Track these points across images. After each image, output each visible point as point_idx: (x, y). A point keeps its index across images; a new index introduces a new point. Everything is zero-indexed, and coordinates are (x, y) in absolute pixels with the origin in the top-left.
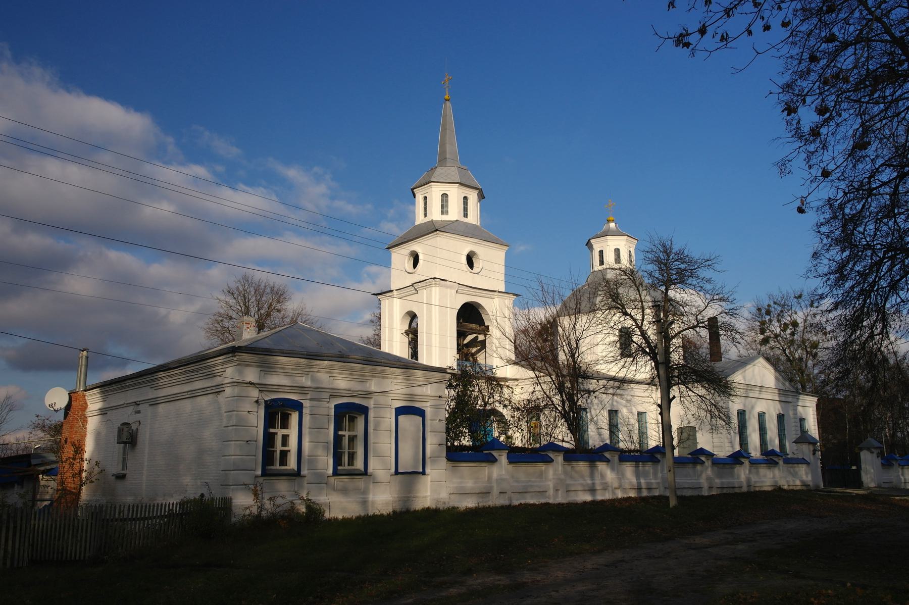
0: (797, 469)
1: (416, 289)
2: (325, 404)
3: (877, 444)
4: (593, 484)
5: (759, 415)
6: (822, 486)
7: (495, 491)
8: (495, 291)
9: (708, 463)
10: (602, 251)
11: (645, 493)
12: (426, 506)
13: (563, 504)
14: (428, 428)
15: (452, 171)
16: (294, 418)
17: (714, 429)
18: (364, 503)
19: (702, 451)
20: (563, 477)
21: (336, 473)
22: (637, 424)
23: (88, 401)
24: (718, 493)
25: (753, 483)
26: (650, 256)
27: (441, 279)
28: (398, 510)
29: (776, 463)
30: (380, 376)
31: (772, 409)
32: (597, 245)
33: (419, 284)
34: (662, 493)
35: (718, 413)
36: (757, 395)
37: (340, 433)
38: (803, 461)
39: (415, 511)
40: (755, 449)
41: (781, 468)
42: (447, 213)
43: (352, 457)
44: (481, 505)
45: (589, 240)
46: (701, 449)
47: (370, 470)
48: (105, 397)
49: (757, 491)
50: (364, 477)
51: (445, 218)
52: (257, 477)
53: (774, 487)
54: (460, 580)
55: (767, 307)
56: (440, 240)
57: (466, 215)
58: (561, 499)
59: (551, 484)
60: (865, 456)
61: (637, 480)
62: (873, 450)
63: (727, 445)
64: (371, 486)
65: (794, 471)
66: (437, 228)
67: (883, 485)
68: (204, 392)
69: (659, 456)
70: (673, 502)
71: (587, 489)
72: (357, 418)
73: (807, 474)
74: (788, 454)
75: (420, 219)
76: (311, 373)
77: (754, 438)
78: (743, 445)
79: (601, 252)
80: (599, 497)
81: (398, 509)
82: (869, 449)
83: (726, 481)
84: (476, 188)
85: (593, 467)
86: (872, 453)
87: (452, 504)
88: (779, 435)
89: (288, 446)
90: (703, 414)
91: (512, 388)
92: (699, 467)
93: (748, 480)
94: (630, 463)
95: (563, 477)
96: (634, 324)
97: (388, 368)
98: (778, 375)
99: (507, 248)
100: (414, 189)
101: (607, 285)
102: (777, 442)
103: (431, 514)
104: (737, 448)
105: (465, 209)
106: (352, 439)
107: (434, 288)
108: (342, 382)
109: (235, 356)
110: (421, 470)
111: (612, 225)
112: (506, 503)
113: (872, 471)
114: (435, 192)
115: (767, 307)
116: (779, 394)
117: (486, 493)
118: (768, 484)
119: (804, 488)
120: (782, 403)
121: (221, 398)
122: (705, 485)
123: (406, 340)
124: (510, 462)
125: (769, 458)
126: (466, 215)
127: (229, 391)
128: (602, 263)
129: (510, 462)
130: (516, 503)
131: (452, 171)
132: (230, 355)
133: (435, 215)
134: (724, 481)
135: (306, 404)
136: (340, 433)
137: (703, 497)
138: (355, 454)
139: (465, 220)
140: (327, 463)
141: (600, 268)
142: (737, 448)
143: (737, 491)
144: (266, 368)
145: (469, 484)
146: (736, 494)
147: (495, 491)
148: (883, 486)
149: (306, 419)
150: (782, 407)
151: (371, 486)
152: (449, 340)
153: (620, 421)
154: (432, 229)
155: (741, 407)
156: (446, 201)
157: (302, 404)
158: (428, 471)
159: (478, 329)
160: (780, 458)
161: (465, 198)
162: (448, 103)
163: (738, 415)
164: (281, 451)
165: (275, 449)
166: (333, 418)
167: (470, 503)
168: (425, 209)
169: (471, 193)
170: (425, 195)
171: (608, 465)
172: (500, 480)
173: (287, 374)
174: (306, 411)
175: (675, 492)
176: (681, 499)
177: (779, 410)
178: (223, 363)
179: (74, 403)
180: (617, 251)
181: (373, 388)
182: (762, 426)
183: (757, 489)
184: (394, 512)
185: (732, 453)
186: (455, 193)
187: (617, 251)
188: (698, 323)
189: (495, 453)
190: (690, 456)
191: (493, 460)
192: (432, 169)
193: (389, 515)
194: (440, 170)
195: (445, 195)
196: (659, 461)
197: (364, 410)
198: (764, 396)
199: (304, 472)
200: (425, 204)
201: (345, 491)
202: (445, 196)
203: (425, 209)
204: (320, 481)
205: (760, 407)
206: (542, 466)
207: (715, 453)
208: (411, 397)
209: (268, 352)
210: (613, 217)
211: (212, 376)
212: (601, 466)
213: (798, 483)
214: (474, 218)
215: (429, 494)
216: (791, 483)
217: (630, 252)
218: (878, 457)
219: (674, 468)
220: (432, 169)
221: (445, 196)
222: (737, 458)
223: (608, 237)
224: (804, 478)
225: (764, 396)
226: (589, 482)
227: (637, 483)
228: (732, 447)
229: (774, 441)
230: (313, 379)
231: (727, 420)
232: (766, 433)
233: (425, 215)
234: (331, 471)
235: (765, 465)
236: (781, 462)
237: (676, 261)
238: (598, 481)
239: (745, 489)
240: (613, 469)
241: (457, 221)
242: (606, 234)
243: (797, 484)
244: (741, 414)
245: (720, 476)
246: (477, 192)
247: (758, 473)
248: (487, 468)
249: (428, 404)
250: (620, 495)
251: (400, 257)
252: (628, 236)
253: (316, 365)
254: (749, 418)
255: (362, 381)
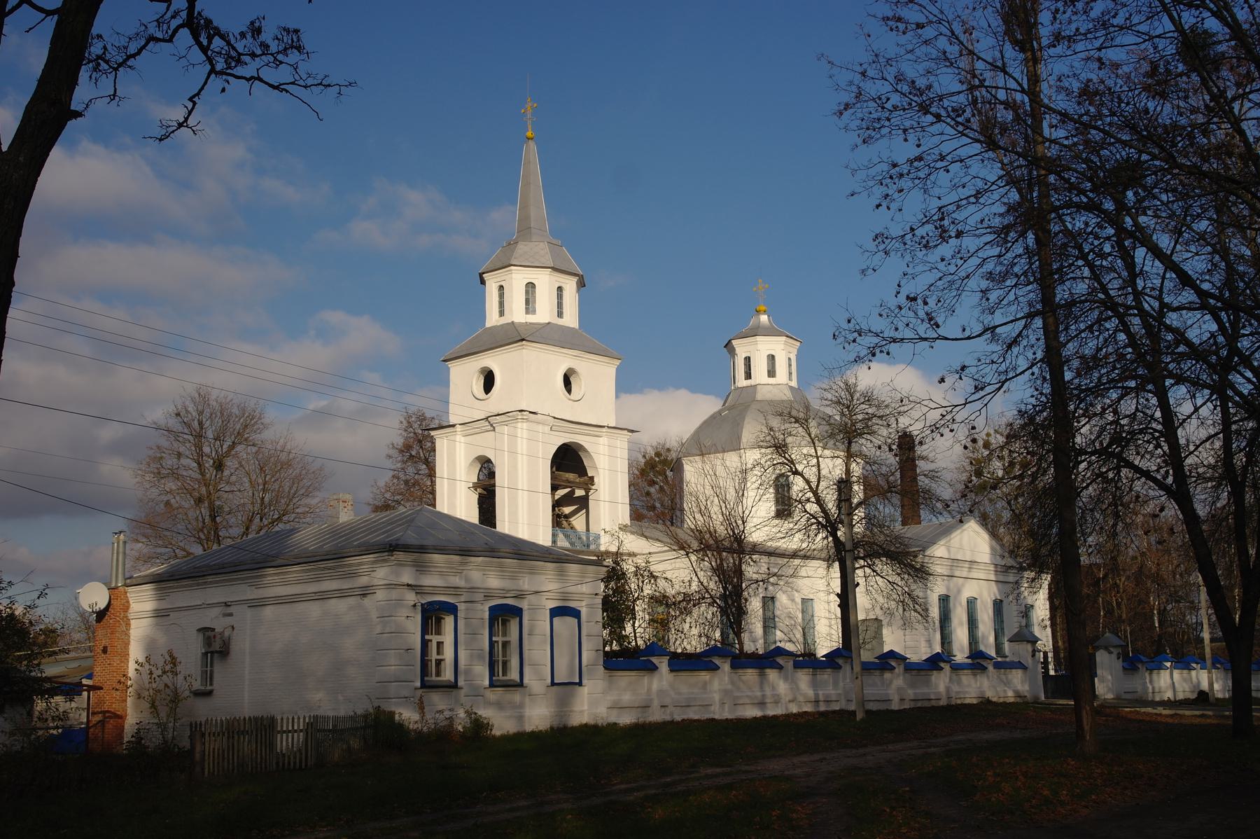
0: (1010, 677)
1: (492, 425)
2: (479, 606)
3: (1116, 641)
4: (764, 696)
5: (968, 602)
6: (1043, 698)
7: (656, 703)
8: (604, 427)
9: (899, 669)
10: (749, 358)
11: (822, 708)
12: (584, 722)
13: (731, 720)
14: (584, 633)
15: (539, 248)
16: (448, 622)
17: (906, 624)
18: (521, 718)
19: (892, 654)
20: (730, 687)
21: (492, 685)
22: (800, 616)
23: (130, 599)
24: (912, 706)
25: (953, 695)
26: (830, 396)
27: (530, 412)
28: (555, 726)
29: (984, 669)
30: (533, 572)
31: (985, 594)
32: (742, 348)
33: (497, 417)
34: (844, 707)
35: (911, 604)
36: (965, 574)
37: (427, 637)
38: (1020, 666)
39: (573, 728)
40: (962, 651)
41: (990, 674)
42: (534, 312)
43: (505, 664)
44: (641, 720)
45: (730, 341)
46: (892, 652)
47: (526, 681)
48: (161, 596)
49: (959, 705)
50: (520, 689)
51: (531, 319)
52: (416, 689)
53: (980, 700)
54: (632, 798)
55: (985, 437)
56: (529, 354)
57: (560, 314)
58: (727, 714)
59: (717, 697)
60: (1101, 657)
61: (814, 690)
62: (1112, 649)
63: (923, 644)
64: (527, 699)
65: (1007, 678)
66: (523, 337)
67: (1124, 696)
68: (342, 594)
69: (840, 661)
70: (860, 716)
71: (756, 702)
72: (509, 621)
73: (1022, 682)
74: (1006, 657)
75: (493, 319)
76: (465, 572)
77: (960, 635)
78: (946, 645)
79: (748, 360)
80: (771, 712)
81: (555, 724)
82: (1106, 648)
83: (922, 691)
84: (575, 275)
85: (762, 675)
86: (1110, 653)
87: (613, 719)
88: (995, 629)
89: (443, 654)
90: (893, 605)
91: (671, 581)
92: (887, 675)
93: (948, 689)
94: (807, 670)
95: (730, 687)
96: (807, 487)
97: (542, 563)
98: (994, 543)
99: (618, 362)
100: (484, 273)
101: (772, 433)
102: (992, 639)
103: (591, 732)
104: (938, 649)
105: (560, 305)
106: (505, 644)
107: (519, 425)
108: (494, 582)
109: (392, 556)
110: (578, 681)
111: (764, 318)
112: (668, 718)
113: (1110, 677)
114: (517, 279)
115: (985, 437)
116: (996, 571)
117: (645, 707)
118: (974, 695)
119: (1018, 700)
120: (1000, 585)
121: (367, 601)
122: (896, 698)
123: (475, 497)
124: (672, 671)
125: (976, 661)
126: (560, 314)
127: (380, 595)
128: (748, 375)
129: (672, 671)
130: (678, 718)
131: (539, 248)
132: (386, 554)
133: (517, 313)
134: (917, 691)
135: (461, 607)
136: (427, 637)
137: (892, 711)
138: (508, 663)
139: (560, 322)
140: (482, 673)
141: (748, 382)
142: (938, 649)
143: (934, 703)
144: (421, 568)
145: (627, 698)
146: (933, 707)
147: (656, 703)
148: (1123, 697)
149: (461, 623)
150: (999, 590)
151: (527, 699)
152: (445, 464)
153: (777, 613)
154: (514, 336)
155: (943, 591)
156: (532, 294)
157: (457, 606)
158: (584, 682)
159: (578, 480)
160: (989, 661)
161: (560, 289)
162: (531, 143)
163: (939, 602)
164: (436, 660)
165: (429, 658)
166: (487, 621)
167: (626, 719)
168: (501, 304)
169: (567, 281)
170: (502, 283)
171: (780, 672)
172: (661, 692)
173: (441, 574)
174: (461, 614)
175: (863, 705)
176: (868, 712)
177: (995, 595)
178: (374, 562)
179: (112, 602)
180: (772, 358)
181: (526, 587)
182: (972, 617)
183: (959, 702)
184: (552, 728)
185: (929, 655)
186: (545, 281)
187: (772, 358)
188: (889, 487)
189: (655, 660)
190: (877, 661)
191: (653, 668)
192: (510, 244)
193: (546, 731)
194: (522, 248)
195: (530, 285)
196: (840, 667)
197: (518, 612)
198: (974, 574)
199: (461, 683)
200: (501, 296)
201: (499, 705)
202: (531, 287)
203: (501, 304)
204: (476, 693)
205: (969, 591)
206: (704, 676)
207: (908, 656)
208: (565, 596)
209: (422, 549)
210: (765, 305)
211: (354, 575)
212: (772, 674)
213: (1010, 693)
214: (571, 319)
215: (586, 708)
216: (1002, 694)
217: (790, 359)
218: (1118, 658)
219: (862, 676)
220: (510, 244)
221: (531, 287)
222: (934, 662)
223: (758, 338)
224: (1019, 687)
225: (974, 574)
226: (759, 694)
227: (815, 694)
228: (930, 646)
229: (988, 639)
230: (467, 580)
231: (925, 613)
232: (977, 627)
233: (502, 313)
234: (487, 683)
235: (969, 671)
236: (991, 668)
237: (863, 403)
238: (768, 692)
239: (943, 702)
240: (786, 679)
241: (549, 323)
242: (755, 332)
243: (1010, 696)
244: (944, 600)
245: (912, 685)
246: (576, 279)
247: (959, 683)
248: (646, 677)
249: (584, 603)
250: (794, 709)
251: (464, 375)
252: (787, 336)
253: (470, 562)
254: (954, 605)
255: (513, 578)
